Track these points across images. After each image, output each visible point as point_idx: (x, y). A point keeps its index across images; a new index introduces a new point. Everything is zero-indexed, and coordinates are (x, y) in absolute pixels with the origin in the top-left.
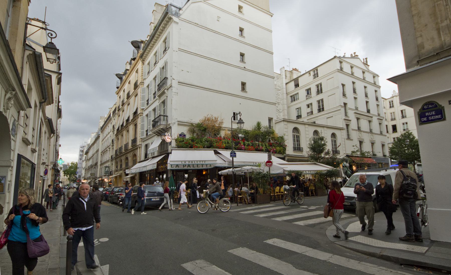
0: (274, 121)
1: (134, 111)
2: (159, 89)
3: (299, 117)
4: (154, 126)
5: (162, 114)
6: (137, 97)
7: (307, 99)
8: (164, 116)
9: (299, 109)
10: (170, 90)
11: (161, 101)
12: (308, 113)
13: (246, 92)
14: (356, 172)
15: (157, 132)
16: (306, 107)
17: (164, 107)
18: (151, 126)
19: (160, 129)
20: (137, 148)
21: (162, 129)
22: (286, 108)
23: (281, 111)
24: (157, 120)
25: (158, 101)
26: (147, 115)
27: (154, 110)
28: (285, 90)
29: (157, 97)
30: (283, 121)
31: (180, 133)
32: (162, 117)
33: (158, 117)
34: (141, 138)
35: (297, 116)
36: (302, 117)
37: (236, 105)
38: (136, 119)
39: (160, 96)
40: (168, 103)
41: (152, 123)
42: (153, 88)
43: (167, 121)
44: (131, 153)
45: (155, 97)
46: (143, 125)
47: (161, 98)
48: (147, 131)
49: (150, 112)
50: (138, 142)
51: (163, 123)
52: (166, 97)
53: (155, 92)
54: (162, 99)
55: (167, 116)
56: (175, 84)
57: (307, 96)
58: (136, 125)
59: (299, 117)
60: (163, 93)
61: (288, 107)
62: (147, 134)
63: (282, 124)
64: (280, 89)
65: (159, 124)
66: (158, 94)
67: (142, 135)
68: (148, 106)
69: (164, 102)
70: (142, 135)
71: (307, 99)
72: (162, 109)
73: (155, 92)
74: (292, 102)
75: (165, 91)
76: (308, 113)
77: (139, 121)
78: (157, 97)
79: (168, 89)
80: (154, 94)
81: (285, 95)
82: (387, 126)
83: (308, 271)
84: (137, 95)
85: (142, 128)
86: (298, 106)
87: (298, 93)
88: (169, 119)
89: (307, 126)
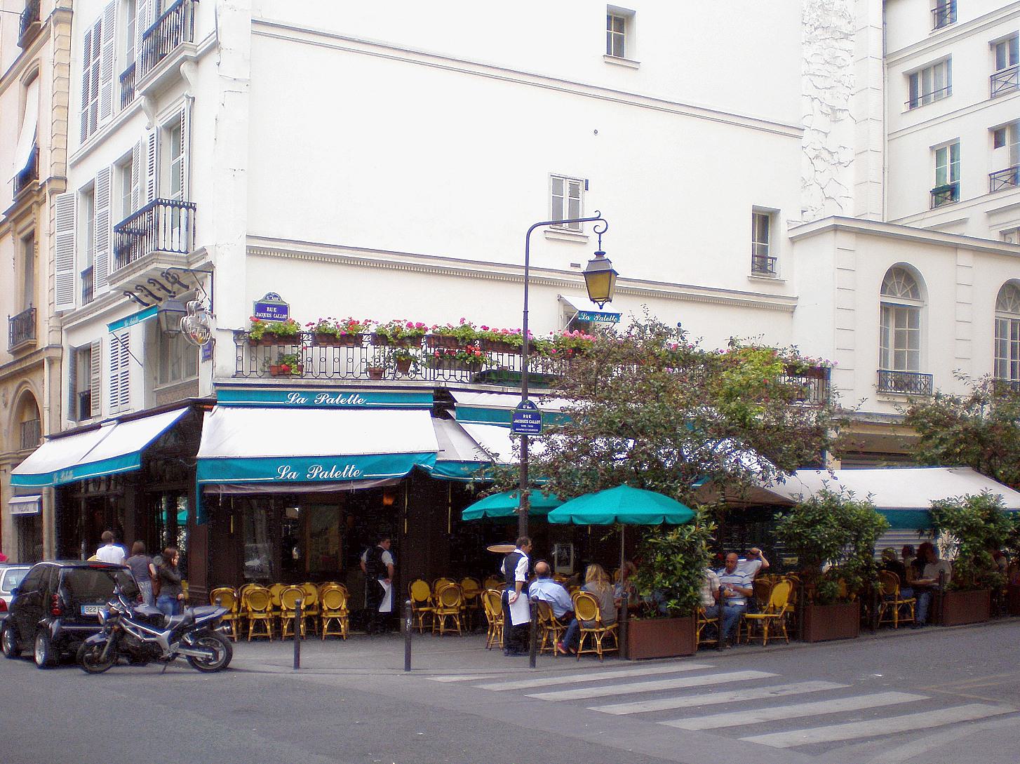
0: (781, 231)
1: (22, 165)
2: (156, 53)
3: (946, 193)
4: (123, 252)
5: (167, 194)
6: (35, 84)
7: (994, 96)
8: (176, 205)
9: (947, 152)
10: (209, 64)
11: (160, 123)
12: (993, 177)
13: (634, 66)
14: (314, 616)
15: (140, 287)
16: (986, 140)
17: (177, 150)
18: (110, 252)
19: (157, 276)
20: (40, 365)
21: (166, 274)
22: (876, 141)
23: (845, 156)
24: (139, 224)
25: (142, 120)
26: (89, 192)
27: (125, 165)
28: (875, 38)
29: (139, 99)
30: (836, 229)
31: (259, 297)
32: (165, 213)
33: (148, 209)
34: (60, 314)
35: (937, 192)
36: (963, 194)
37: (574, 138)
38: (29, 211)
39: (156, 96)
40: (202, 131)
41: (112, 238)
42: (124, 48)
43: (191, 229)
44: (12, 388)
45: (127, 96)
46: (66, 245)
47: (164, 104)
48: (88, 274)
49: (104, 174)
50: (45, 336)
51: (171, 240)
52: (185, 105)
53: (132, 68)
54: (172, 107)
55: (191, 207)
56: (235, 37)
57: (993, 79)
58: (29, 240)
59: (946, 193)
60: (174, 80)
61: (891, 137)
62: (88, 292)
63: (831, 243)
64: (847, 29)
65: (149, 248)
66: (146, 80)
67: (65, 296)
68: (93, 139)
69: (174, 129)
70: (65, 296)
71: (994, 96)
72: (168, 163)
73: (132, 68)
74: (913, 104)
75: (184, 68)
76: (993, 177)
77: (46, 219)
78: (139, 99)
79: (197, 61)
80: (127, 76)
81: (876, 66)
82: (254, 22)
83: (299, 663)
84: (35, 75)
85: (65, 260)
86: (942, 135)
87: (947, 61)
88: (203, 218)
89: (964, 258)
